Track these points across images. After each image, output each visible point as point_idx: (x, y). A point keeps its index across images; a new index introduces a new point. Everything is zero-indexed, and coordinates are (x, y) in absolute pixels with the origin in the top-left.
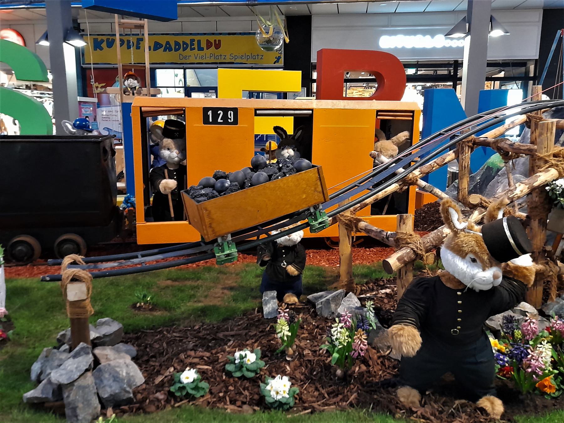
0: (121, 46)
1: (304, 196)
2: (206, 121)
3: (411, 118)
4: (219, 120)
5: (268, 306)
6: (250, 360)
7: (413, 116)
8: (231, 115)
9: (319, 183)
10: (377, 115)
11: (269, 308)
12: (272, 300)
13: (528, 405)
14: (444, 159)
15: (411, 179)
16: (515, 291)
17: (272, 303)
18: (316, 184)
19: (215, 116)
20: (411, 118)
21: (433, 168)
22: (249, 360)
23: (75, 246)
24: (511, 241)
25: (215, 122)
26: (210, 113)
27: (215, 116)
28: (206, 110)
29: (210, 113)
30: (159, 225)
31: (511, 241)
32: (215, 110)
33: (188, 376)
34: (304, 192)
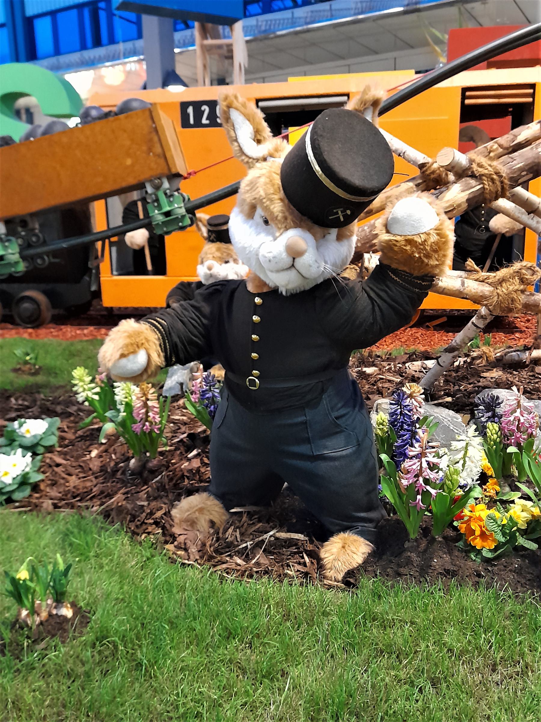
0: (528, 190)
1: (129, 162)
2: (185, 124)
3: (531, 100)
4: (204, 121)
5: (173, 378)
6: (30, 430)
7: (533, 95)
8: (206, 109)
9: (156, 139)
10: (464, 97)
11: (172, 382)
12: (181, 371)
13: (409, 562)
14: (516, 136)
15: (433, 172)
16: (388, 295)
17: (179, 374)
18: (151, 140)
19: (198, 114)
20: (531, 100)
21: (490, 153)
22: (28, 431)
23: (35, 306)
24: (317, 168)
25: (198, 124)
26: (190, 110)
27: (198, 114)
28: (184, 106)
29: (190, 110)
30: (137, 280)
31: (317, 168)
32: (197, 105)
33: (8, 471)
34: (128, 155)
